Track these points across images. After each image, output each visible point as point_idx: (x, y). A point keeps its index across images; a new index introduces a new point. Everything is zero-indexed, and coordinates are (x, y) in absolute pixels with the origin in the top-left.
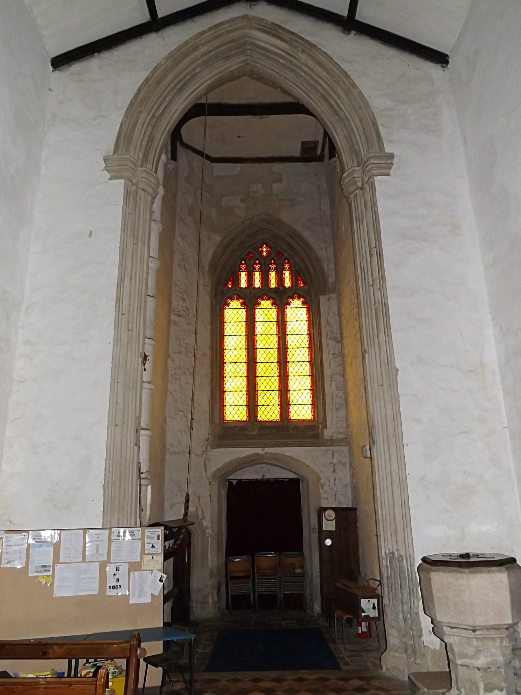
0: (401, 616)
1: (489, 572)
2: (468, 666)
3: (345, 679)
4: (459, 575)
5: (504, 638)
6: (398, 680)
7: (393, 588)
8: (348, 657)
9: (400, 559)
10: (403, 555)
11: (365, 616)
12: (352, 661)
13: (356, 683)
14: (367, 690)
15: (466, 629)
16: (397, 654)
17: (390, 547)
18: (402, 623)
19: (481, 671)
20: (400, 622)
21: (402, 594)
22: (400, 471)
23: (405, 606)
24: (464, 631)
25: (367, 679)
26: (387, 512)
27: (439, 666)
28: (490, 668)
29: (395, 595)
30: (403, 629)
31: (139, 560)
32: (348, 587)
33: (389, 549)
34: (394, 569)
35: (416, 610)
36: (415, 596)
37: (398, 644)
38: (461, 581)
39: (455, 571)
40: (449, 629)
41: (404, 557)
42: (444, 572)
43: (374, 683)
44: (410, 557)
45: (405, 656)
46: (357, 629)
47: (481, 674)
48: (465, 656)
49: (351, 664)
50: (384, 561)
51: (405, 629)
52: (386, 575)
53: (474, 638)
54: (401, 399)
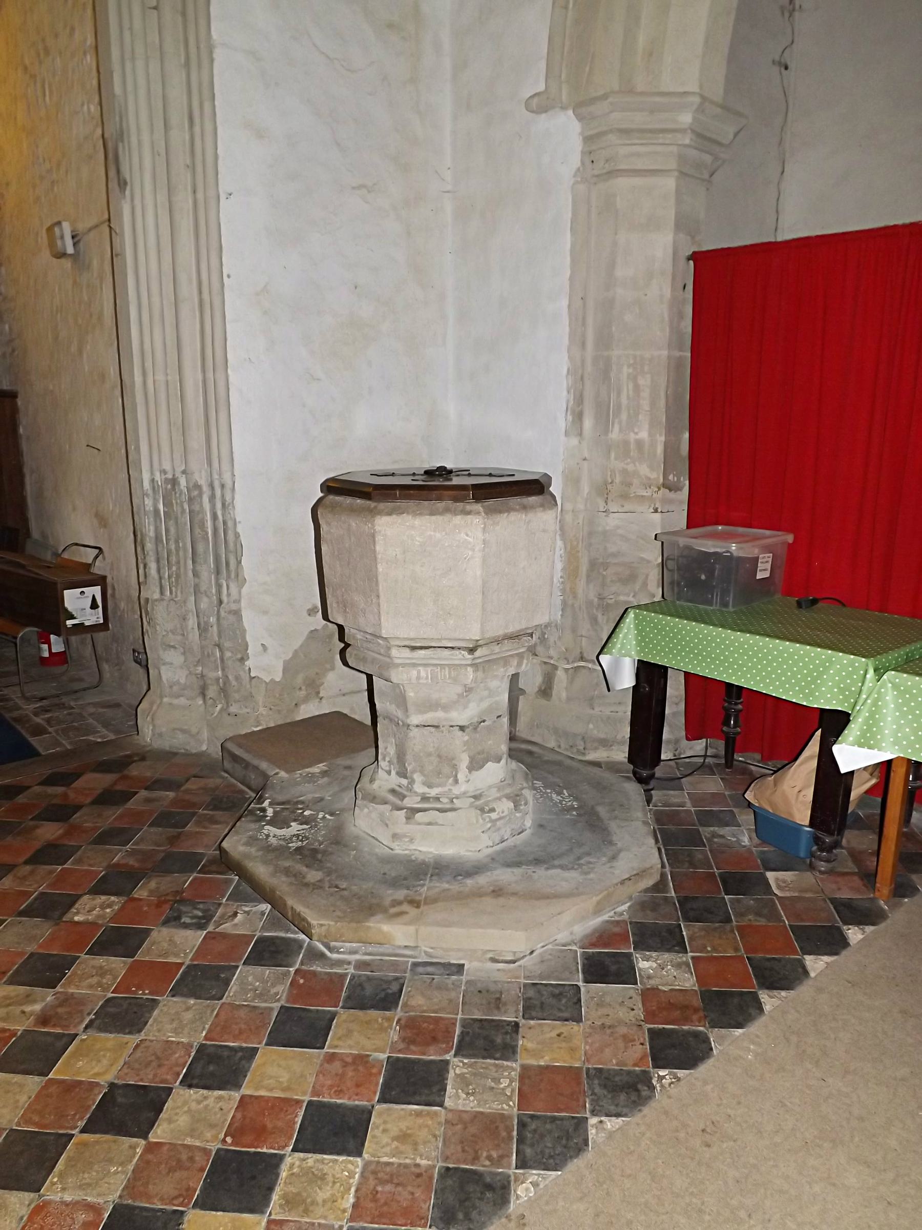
0: (192, 622)
1: (525, 508)
2: (437, 727)
3: (65, 779)
4: (458, 520)
5: (525, 656)
6: (188, 755)
7: (174, 559)
8: (36, 714)
9: (196, 493)
10: (203, 482)
11: (74, 625)
12: (48, 721)
13: (96, 782)
14: (127, 796)
15: (453, 648)
16: (182, 701)
17: (167, 466)
18: (194, 636)
19: (467, 730)
20: (190, 636)
21: (196, 574)
22: (204, 266)
23: (205, 599)
24: (447, 652)
25: (120, 765)
26: (160, 377)
27: (279, 712)
28: (484, 721)
29: (178, 576)
30: (196, 648)
31: (90, 562)
32: (23, 567)
33: (164, 472)
34: (176, 518)
35: (234, 607)
36: (233, 575)
37: (183, 681)
38: (463, 535)
39: (447, 510)
40: (407, 653)
41: (205, 488)
42: (415, 514)
43: (134, 771)
44: (223, 486)
45: (201, 702)
46: (40, 649)
47: (466, 738)
48: (434, 706)
49: (50, 729)
50: (149, 502)
51: (202, 648)
52: (152, 534)
53: (471, 665)
54: (218, 54)
